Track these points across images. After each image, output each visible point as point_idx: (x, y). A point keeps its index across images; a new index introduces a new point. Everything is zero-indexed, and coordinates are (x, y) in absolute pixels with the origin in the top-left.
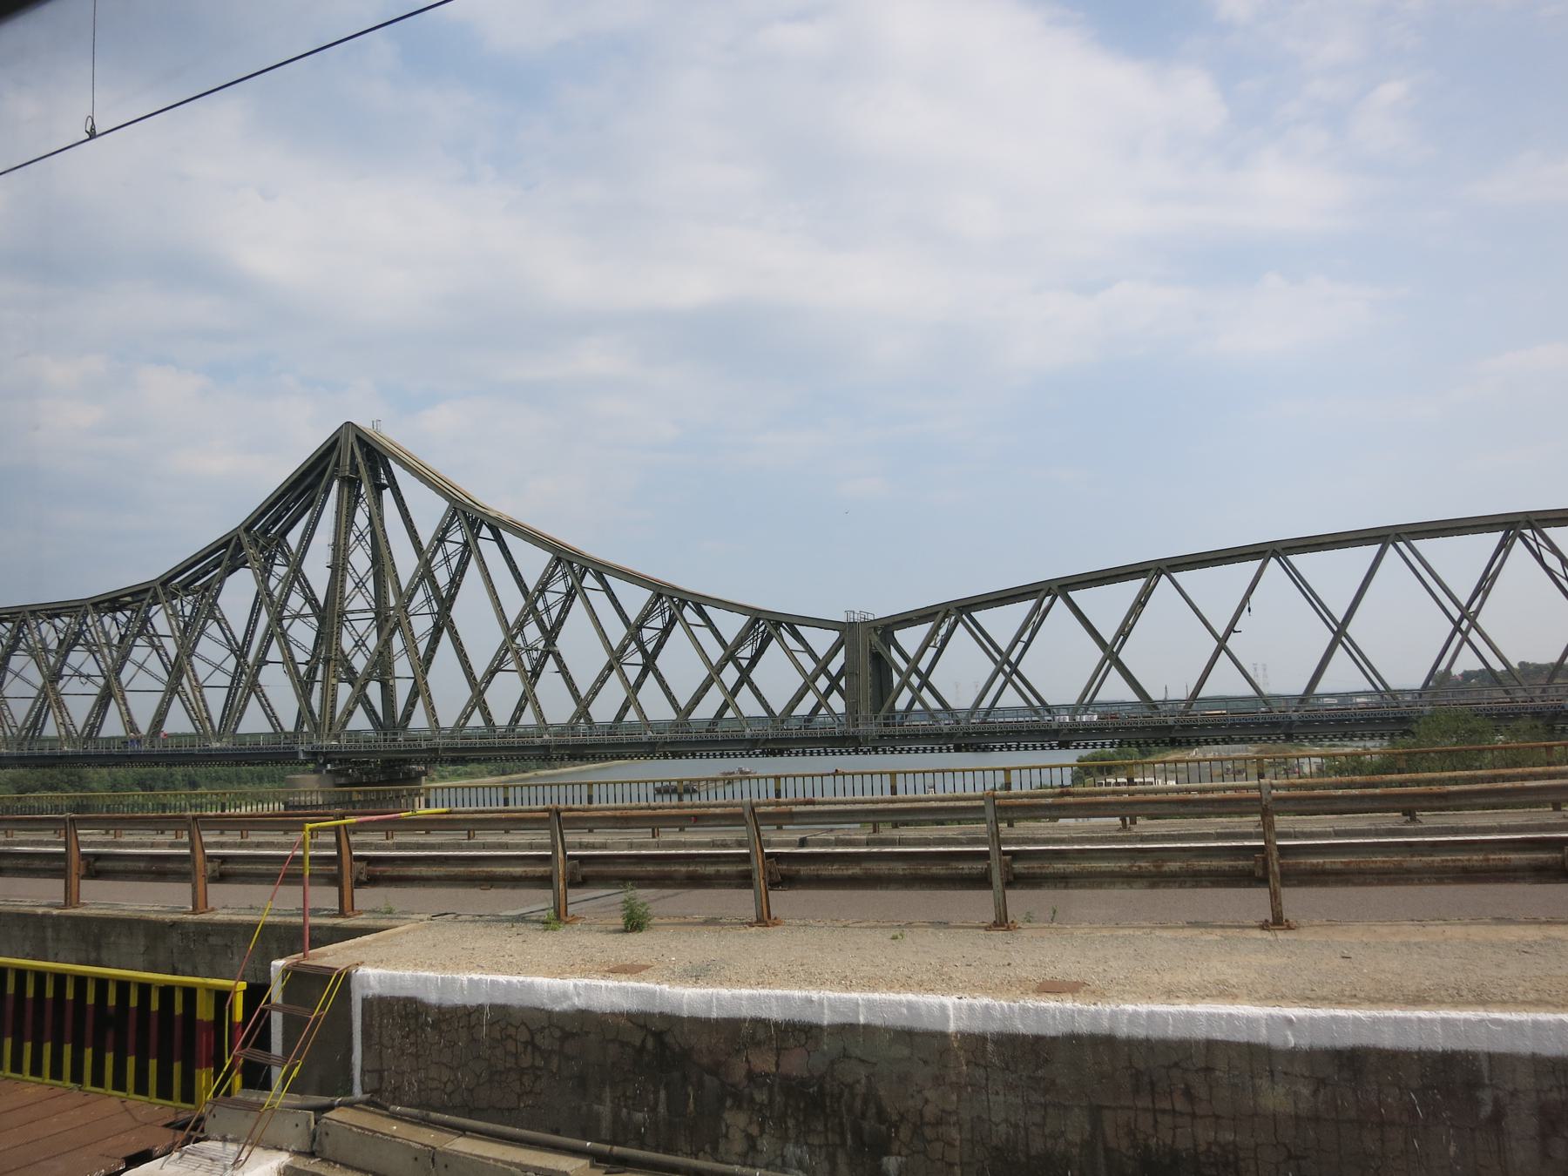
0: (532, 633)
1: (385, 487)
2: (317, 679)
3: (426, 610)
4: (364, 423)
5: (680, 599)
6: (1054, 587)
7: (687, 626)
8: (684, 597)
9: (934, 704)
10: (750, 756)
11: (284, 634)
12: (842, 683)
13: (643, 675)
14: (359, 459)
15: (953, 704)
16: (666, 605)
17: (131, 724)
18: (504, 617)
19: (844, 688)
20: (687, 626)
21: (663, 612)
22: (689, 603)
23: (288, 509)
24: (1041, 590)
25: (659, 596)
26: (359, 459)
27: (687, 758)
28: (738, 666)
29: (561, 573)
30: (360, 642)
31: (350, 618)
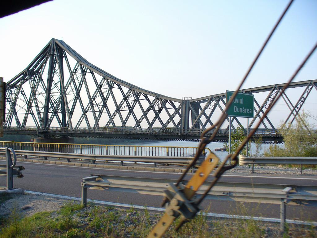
0: (99, 100)
1: (63, 57)
2: (50, 111)
3: (72, 93)
4: (58, 37)
5: (165, 100)
6: (312, 83)
7: (166, 109)
8: (166, 99)
9: (269, 127)
10: (189, 141)
11: (36, 99)
12: (180, 111)
13: (129, 115)
14: (55, 47)
15: (276, 128)
16: (160, 102)
17: (18, 122)
18: (116, 102)
19: (181, 113)
20: (166, 109)
21: (159, 104)
22: (168, 101)
23: (39, 63)
24: (308, 83)
25: (158, 99)
26: (55, 47)
27: (175, 141)
28: (155, 111)
29: (157, 103)
30: (55, 102)
31: (115, 108)
